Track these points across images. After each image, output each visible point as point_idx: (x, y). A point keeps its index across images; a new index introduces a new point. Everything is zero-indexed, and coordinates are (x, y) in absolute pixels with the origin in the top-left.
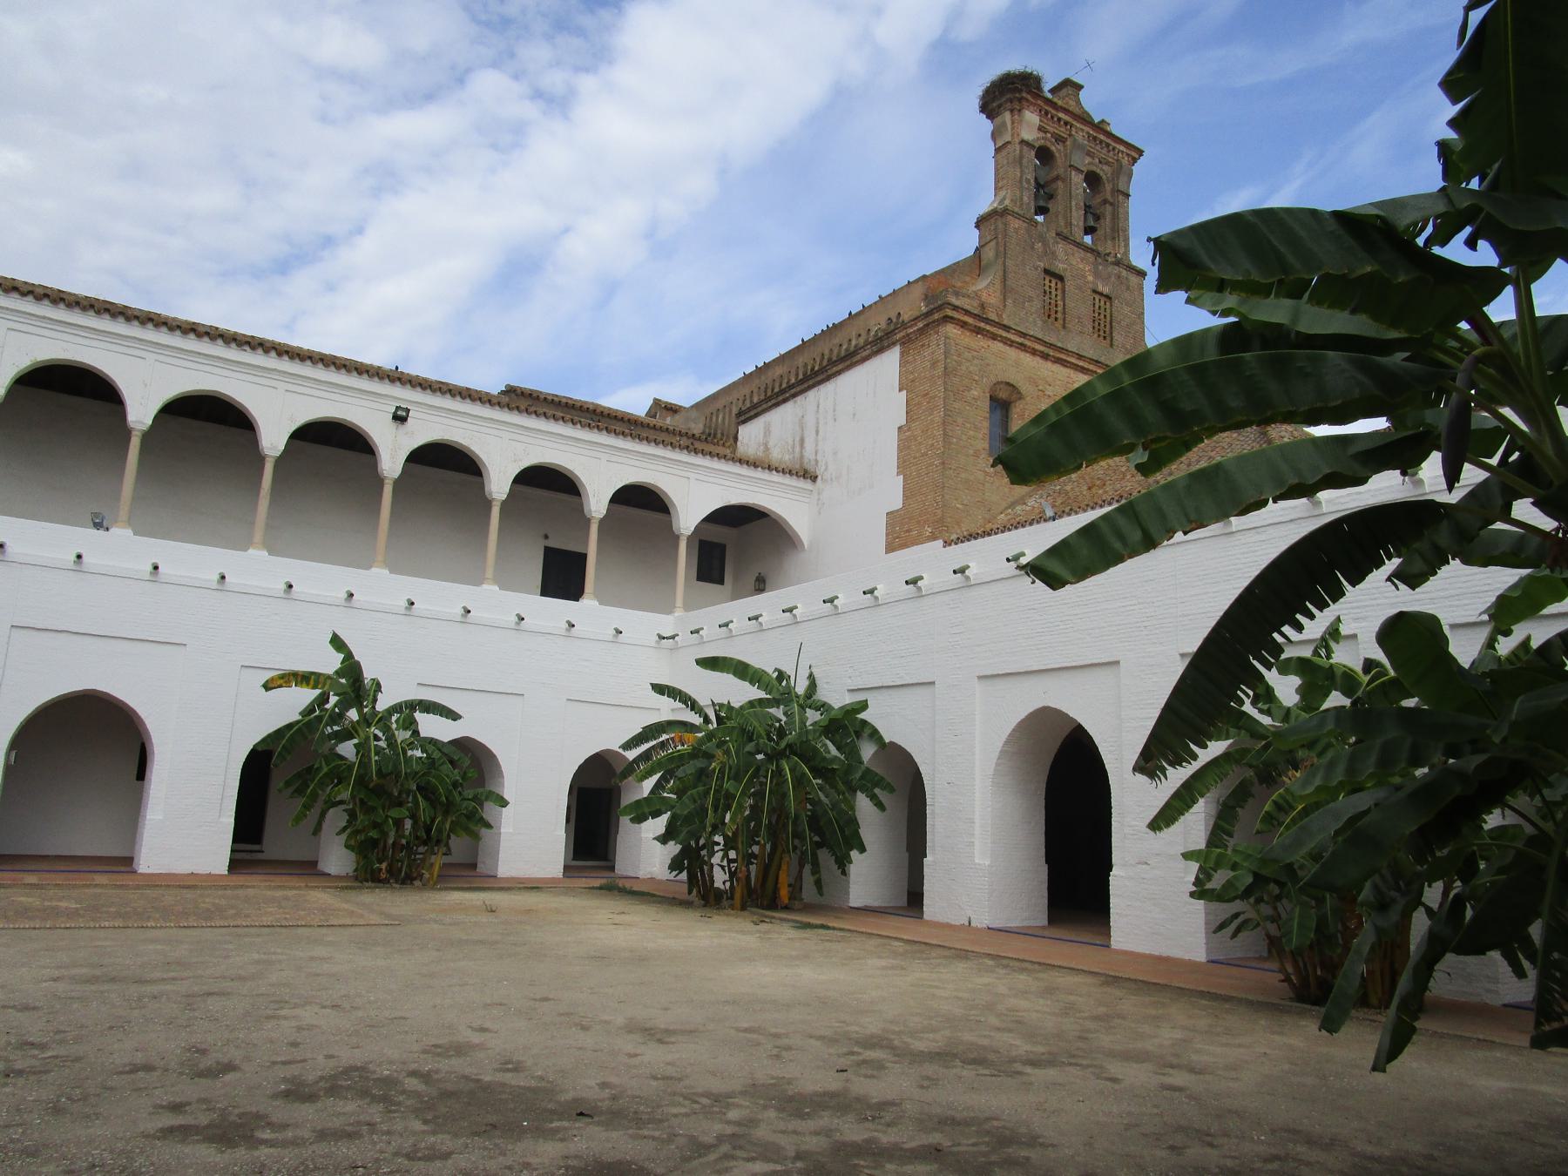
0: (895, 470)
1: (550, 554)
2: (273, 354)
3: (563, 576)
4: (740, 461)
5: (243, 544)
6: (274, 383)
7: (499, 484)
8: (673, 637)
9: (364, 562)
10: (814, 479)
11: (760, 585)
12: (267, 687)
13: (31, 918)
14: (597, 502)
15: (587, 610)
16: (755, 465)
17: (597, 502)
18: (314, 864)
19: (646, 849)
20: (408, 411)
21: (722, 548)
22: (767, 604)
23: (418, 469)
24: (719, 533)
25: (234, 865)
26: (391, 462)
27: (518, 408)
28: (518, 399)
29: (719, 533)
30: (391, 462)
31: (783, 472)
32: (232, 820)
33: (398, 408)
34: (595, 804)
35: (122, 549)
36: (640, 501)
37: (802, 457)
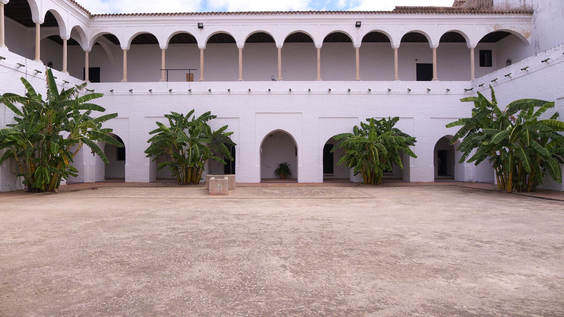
0: (398, 5)
1: (418, 66)
2: (314, 13)
3: (424, 73)
4: (495, 13)
5: (315, 79)
6: (316, 23)
7: (396, 42)
8: (471, 89)
9: (234, 78)
10: (531, 12)
11: (509, 62)
12: (447, 126)
13: (266, 195)
14: (435, 42)
15: (436, 85)
16: (503, 13)
17: (435, 42)
18: (349, 179)
19: (469, 169)
20: (360, 22)
21: (490, 52)
22: (514, 69)
23: (442, 43)
24: (487, 46)
25: (325, 180)
26: (357, 42)
27: (453, 12)
28: (399, 10)
29: (487, 46)
30: (357, 42)
31: (516, 13)
32: (322, 166)
33: (199, 24)
34: (445, 154)
35: (280, 86)
36: (453, 38)
37: (525, 6)
